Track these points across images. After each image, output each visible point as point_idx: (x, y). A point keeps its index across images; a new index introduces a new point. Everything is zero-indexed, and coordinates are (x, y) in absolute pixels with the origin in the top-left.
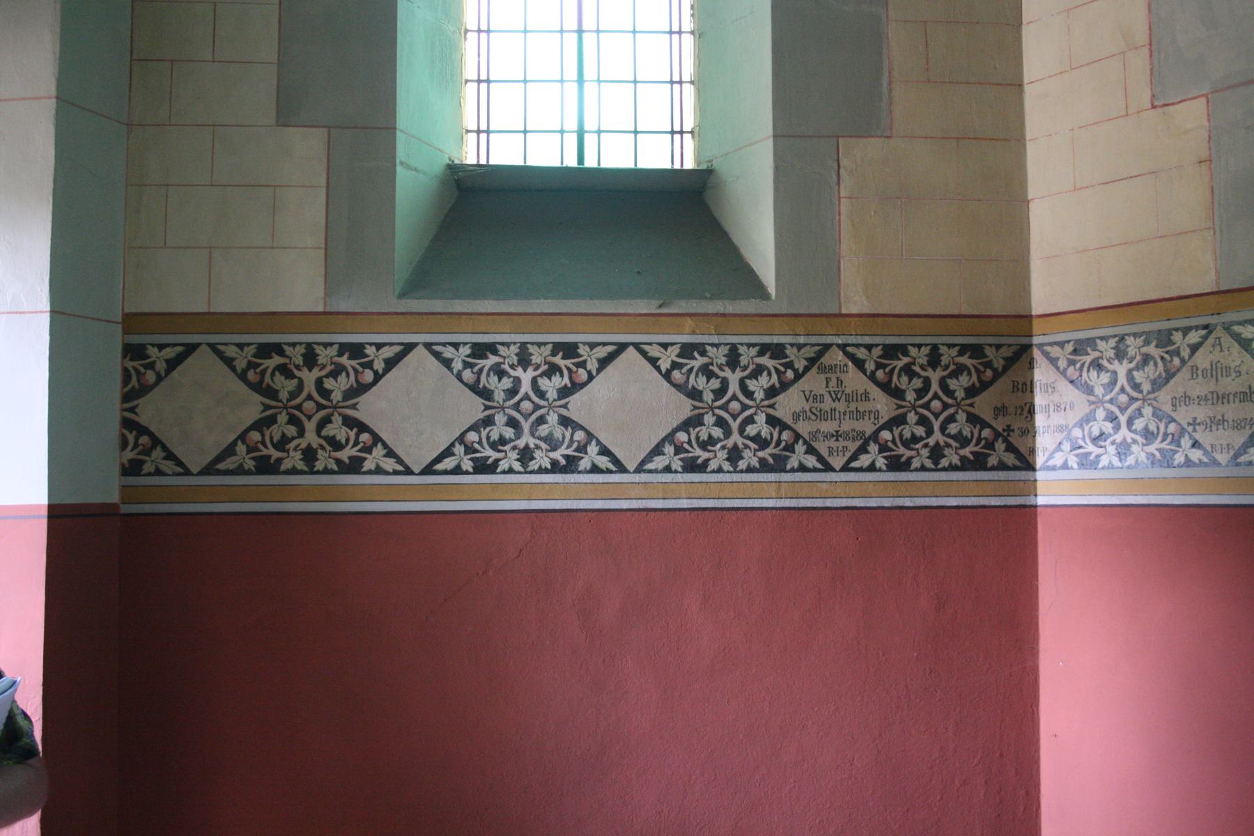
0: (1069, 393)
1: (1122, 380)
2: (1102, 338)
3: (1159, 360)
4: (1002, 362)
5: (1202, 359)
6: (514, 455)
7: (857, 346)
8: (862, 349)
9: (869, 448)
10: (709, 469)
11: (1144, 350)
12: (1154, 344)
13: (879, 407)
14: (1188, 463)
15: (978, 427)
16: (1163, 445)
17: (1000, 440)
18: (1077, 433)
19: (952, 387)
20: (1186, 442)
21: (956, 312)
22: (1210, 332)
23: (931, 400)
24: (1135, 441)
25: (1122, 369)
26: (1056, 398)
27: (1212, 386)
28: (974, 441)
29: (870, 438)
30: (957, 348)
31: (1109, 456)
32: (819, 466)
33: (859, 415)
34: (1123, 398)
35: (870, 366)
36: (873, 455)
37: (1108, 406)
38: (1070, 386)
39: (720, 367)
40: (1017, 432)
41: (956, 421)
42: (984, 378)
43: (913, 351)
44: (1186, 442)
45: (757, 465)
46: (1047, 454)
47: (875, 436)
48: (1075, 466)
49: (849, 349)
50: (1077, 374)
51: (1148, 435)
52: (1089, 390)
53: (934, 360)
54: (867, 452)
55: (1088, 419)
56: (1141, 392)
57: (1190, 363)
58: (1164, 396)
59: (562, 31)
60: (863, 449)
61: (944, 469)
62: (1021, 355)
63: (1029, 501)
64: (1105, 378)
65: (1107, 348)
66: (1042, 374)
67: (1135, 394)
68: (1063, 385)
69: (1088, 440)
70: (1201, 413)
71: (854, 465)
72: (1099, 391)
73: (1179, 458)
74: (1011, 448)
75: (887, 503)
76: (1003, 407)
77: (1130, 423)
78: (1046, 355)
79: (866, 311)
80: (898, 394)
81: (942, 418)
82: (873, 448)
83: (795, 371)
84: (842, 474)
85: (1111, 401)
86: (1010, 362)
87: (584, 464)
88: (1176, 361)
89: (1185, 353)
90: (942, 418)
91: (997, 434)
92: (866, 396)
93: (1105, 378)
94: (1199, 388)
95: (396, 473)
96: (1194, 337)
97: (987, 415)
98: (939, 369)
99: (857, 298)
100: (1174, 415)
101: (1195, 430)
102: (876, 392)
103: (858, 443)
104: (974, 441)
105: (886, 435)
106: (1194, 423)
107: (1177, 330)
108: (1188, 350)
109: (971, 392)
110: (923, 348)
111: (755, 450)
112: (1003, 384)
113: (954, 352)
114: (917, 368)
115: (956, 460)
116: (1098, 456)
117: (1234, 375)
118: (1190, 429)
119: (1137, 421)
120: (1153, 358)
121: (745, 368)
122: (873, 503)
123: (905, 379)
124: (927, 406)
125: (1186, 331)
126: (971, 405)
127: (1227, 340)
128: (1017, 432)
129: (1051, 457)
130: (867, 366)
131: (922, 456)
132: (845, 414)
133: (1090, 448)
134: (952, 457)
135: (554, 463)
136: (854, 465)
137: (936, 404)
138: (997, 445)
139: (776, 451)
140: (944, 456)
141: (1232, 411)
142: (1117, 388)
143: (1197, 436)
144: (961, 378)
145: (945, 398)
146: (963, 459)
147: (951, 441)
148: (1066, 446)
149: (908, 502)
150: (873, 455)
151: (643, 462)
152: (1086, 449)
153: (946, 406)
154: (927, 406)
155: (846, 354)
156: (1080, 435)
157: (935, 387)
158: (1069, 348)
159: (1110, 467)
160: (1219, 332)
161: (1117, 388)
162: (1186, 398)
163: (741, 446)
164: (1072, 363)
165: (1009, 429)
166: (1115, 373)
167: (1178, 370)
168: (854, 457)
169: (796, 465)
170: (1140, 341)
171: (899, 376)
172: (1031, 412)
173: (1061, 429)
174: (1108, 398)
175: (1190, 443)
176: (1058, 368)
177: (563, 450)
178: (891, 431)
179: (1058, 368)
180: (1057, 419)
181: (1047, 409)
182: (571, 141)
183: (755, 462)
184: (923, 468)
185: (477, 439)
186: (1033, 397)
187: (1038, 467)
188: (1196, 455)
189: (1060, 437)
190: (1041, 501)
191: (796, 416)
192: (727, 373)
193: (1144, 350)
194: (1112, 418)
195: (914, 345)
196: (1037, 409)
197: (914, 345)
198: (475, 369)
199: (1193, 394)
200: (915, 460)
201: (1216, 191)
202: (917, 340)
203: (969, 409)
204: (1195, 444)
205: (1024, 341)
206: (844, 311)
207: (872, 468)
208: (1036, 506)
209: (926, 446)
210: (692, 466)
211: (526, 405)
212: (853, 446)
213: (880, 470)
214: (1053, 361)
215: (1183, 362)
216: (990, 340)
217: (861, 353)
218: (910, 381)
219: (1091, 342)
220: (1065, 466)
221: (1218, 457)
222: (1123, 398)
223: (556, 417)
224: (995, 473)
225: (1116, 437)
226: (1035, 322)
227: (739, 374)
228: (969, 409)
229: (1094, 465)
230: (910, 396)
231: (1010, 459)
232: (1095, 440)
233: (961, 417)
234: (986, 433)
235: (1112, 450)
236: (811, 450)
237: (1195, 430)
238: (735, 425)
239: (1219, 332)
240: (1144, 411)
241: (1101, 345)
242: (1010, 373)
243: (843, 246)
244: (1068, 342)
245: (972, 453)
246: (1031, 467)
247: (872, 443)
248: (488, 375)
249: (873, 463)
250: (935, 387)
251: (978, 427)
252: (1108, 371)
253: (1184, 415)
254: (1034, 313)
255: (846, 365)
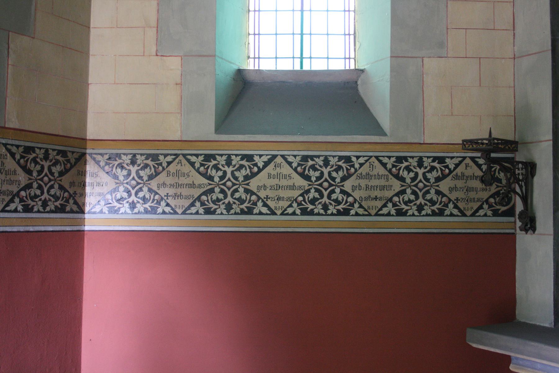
0: (105, 178)
1: (133, 174)
2: (124, 154)
3: (152, 167)
4: (74, 160)
5: (172, 168)
6: (415, 208)
7: (12, 145)
8: (14, 147)
9: (388, 205)
10: (408, 214)
11: (145, 162)
12: (150, 159)
13: (20, 178)
14: (164, 213)
15: (441, 196)
16: (152, 205)
17: (72, 198)
18: (109, 197)
19: (53, 171)
20: (163, 203)
21: (57, 133)
22: (177, 157)
23: (44, 177)
24: (138, 202)
25: (134, 169)
26: (98, 180)
27: (176, 180)
28: (247, 202)
29: (15, 194)
30: (56, 151)
31: (125, 208)
32: (269, 212)
33: (11, 182)
34: (134, 183)
35: (18, 157)
36: (16, 204)
37: (126, 185)
38: (106, 175)
39: (223, 166)
40: (78, 195)
41: (54, 188)
42: (67, 168)
43: (37, 151)
44: (163, 203)
45: (239, 212)
46: (91, 206)
47: (18, 194)
48: (107, 212)
49: (8, 146)
50: (110, 169)
51: (144, 199)
52: (116, 177)
53: (46, 157)
54: (14, 202)
55: (115, 190)
56: (143, 180)
57: (167, 169)
58: (154, 184)
59: (293, 10)
60: (12, 201)
61: (48, 212)
62: (81, 158)
63: (81, 228)
64: (125, 172)
65: (127, 159)
66: (90, 167)
67: (140, 181)
68: (102, 174)
69: (114, 201)
70: (171, 191)
71: (7, 209)
72: (121, 178)
73: (160, 210)
74: (76, 203)
75: (22, 229)
76: (74, 182)
77: (136, 194)
78: (94, 159)
79: (17, 127)
80: (29, 172)
81: (48, 186)
82: (17, 200)
83: (258, 168)
84: (470, 218)
85: (127, 183)
86: (78, 160)
87: (447, 212)
88: (161, 168)
89: (165, 165)
90: (48, 186)
91: (70, 196)
92: (15, 172)
93: (125, 172)
94: (169, 180)
95: (363, 215)
96: (169, 159)
97: (67, 186)
98: (48, 161)
99: (13, 120)
100: (158, 191)
101: (167, 199)
102: (19, 170)
103: (10, 197)
104: (247, 202)
105: (23, 193)
106: (167, 195)
107: (162, 154)
108: (166, 164)
109: (61, 174)
110: (42, 150)
111: (430, 206)
112: (74, 171)
113: (143, 157)
114: (38, 160)
115: (53, 208)
116: (119, 208)
117: (186, 176)
118: (166, 198)
119: (140, 193)
120: (60, 162)
121: (234, 166)
122: (15, 229)
123: (33, 165)
124: (42, 179)
125: (166, 156)
126: (61, 180)
127: (184, 161)
128: (78, 195)
129: (94, 207)
130: (16, 156)
131: (38, 206)
132: (4, 181)
133: (116, 204)
134: (427, 210)
135: (242, 210)
136: (7, 209)
137: (46, 179)
138: (258, 203)
139: (440, 207)
140: (48, 205)
141: (185, 191)
142: (131, 177)
143: (168, 201)
144: (57, 166)
145: (50, 176)
146: (56, 207)
147: (51, 198)
148: (102, 203)
149: (31, 229)
150: (16, 204)
151: (186, 210)
152: (108, 203)
153: (50, 180)
154: (42, 179)
155: (7, 149)
156: (111, 198)
157: (46, 170)
158: (107, 157)
159: (125, 213)
160: (181, 157)
161: (131, 177)
162: (164, 184)
163: (232, 202)
164: (107, 164)
165: (75, 193)
166: (130, 170)
167: (161, 172)
168: (7, 205)
169: (449, 213)
170: (143, 157)
171: (31, 163)
172: (84, 185)
173: (100, 194)
174: (125, 182)
175: (165, 204)
176: (100, 166)
177: (437, 206)
178: (26, 192)
179: (100, 166)
180: (97, 189)
181: (92, 185)
182: (298, 61)
183: (429, 212)
184: (39, 212)
185: (398, 200)
186: (85, 179)
187: (86, 212)
188: (168, 209)
189: (99, 198)
190: (87, 228)
191: (259, 188)
192: (226, 168)
193: (145, 162)
194: (129, 192)
195: (38, 148)
196: (87, 184)
197: (38, 148)
198: (398, 168)
199: (168, 183)
200: (35, 207)
201: (183, 99)
202: (40, 145)
203: (60, 182)
204: (168, 205)
205: (83, 151)
206: (7, 126)
207: (16, 211)
208: (84, 231)
209: (40, 200)
210: (208, 211)
211: (421, 185)
212: (7, 199)
213: (19, 212)
214: (98, 163)
215: (164, 169)
216: (70, 149)
217: (14, 149)
218: (35, 166)
219: (119, 156)
220: (101, 212)
221: (178, 210)
222: (134, 183)
223: (434, 191)
224: (69, 214)
225: (42, 197)
226: (88, 142)
227: (231, 169)
228: (60, 182)
229: (116, 211)
230: (35, 174)
231: (75, 208)
232: (118, 201)
233: (56, 186)
234: (66, 194)
235: (127, 205)
236: (265, 205)
237: (167, 199)
238: (229, 193)
239: (181, 157)
240: (144, 189)
241: (124, 157)
242: (77, 166)
243: (8, 91)
244: (106, 154)
245: (60, 204)
246: (83, 212)
247: (16, 198)
248: (403, 171)
249: (16, 208)
250: (46, 170)
251: (441, 196)
252: (126, 169)
253: (163, 192)
254: (88, 138)
255: (6, 155)
